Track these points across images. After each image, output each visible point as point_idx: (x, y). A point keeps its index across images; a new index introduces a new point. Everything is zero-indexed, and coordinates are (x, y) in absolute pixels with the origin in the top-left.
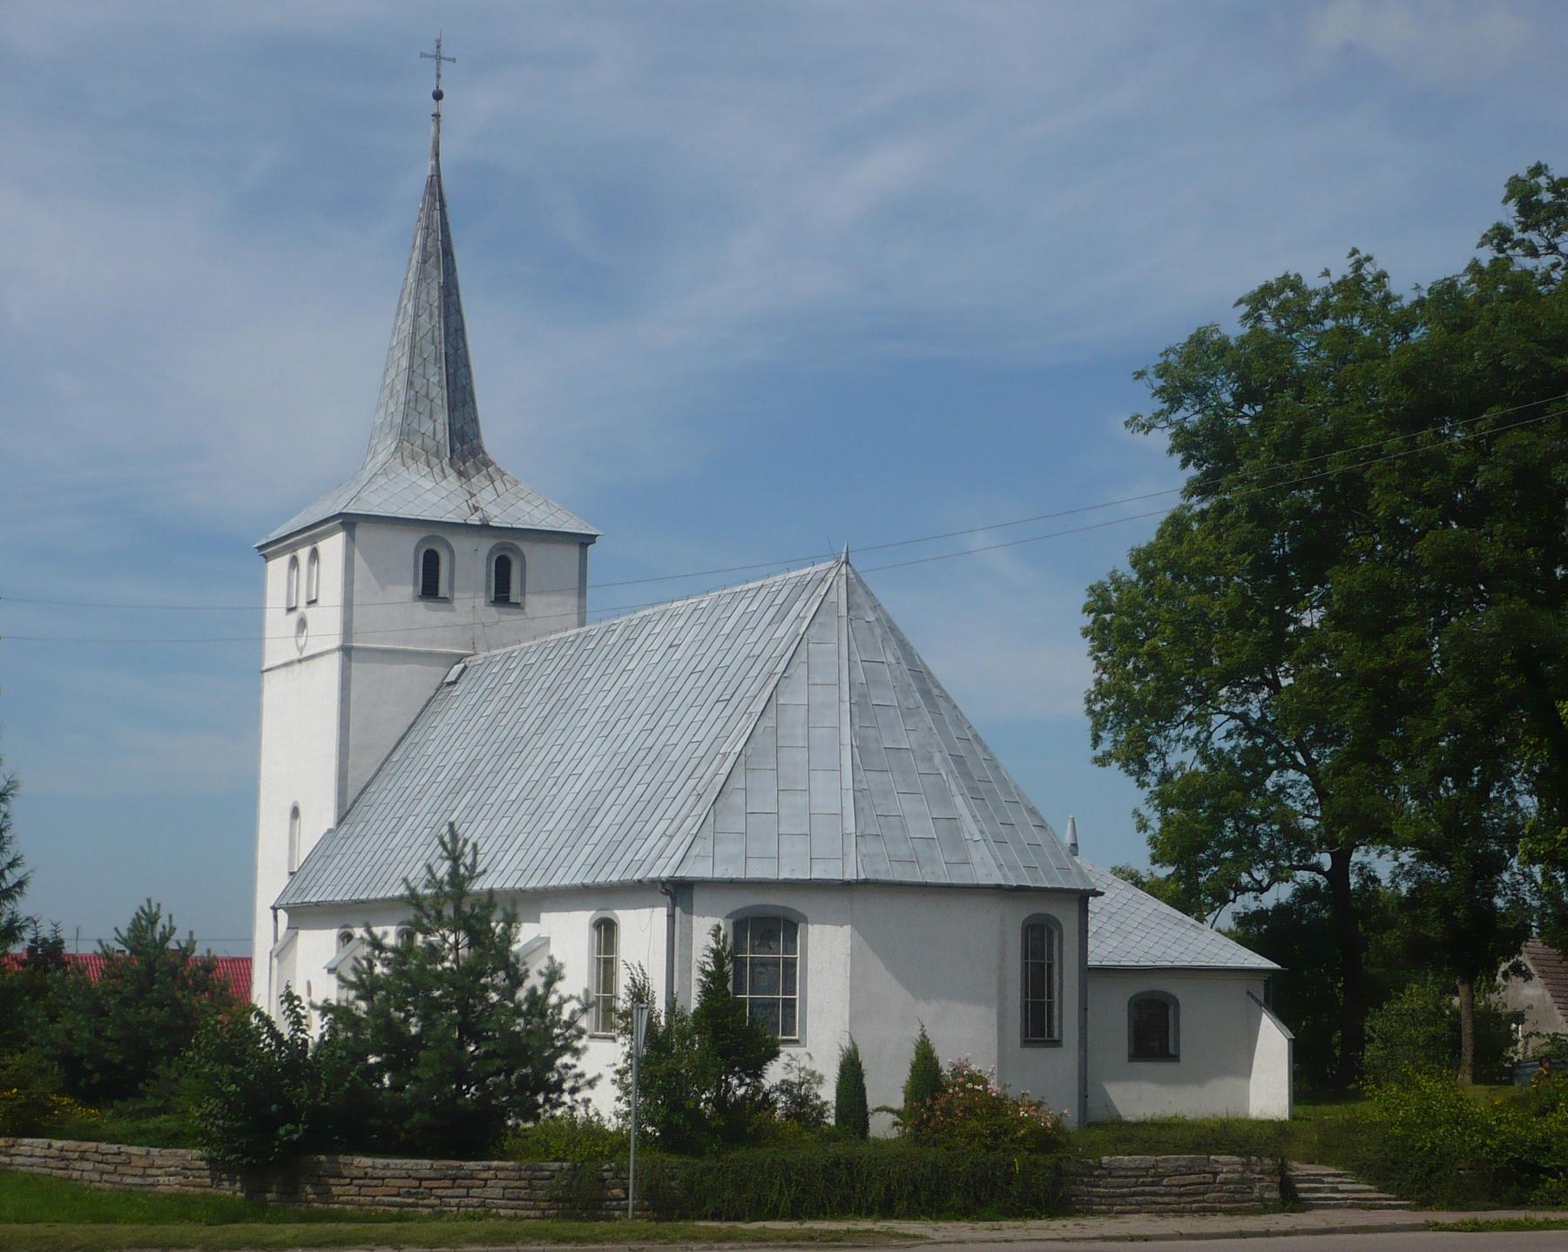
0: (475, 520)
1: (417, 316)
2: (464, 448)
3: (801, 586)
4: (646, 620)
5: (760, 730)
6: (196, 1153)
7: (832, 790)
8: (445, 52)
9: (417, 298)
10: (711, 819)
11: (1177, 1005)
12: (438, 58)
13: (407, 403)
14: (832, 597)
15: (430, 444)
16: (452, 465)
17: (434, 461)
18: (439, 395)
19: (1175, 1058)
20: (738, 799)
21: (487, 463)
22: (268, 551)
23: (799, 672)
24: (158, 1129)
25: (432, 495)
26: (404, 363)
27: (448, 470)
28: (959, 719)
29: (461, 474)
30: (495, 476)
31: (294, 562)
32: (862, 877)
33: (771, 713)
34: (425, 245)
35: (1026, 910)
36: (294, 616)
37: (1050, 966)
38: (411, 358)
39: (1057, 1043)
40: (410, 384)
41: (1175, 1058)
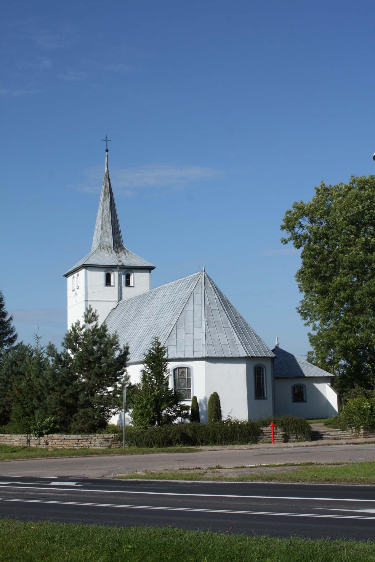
0: (120, 264)
1: (103, 210)
2: (118, 245)
3: (194, 279)
4: (159, 289)
5: (180, 317)
6: (23, 435)
7: (199, 333)
8: (108, 138)
9: (103, 205)
10: (167, 342)
11: (305, 387)
12: (106, 140)
13: (101, 234)
14: (200, 281)
15: (108, 244)
16: (114, 249)
17: (109, 249)
18: (110, 231)
19: (306, 401)
20: (174, 336)
21: (124, 249)
22: (67, 276)
23: (191, 301)
24: (109, 433)
25: (109, 258)
26: (101, 223)
27: (113, 251)
28: (236, 313)
29: (116, 252)
30: (126, 252)
31: (74, 277)
32: (207, 356)
33: (183, 313)
34: (105, 192)
35: (255, 363)
36: (74, 292)
37: (263, 378)
38: (102, 222)
39: (266, 398)
40: (102, 228)
41: (306, 401)
